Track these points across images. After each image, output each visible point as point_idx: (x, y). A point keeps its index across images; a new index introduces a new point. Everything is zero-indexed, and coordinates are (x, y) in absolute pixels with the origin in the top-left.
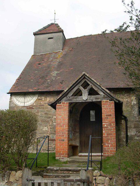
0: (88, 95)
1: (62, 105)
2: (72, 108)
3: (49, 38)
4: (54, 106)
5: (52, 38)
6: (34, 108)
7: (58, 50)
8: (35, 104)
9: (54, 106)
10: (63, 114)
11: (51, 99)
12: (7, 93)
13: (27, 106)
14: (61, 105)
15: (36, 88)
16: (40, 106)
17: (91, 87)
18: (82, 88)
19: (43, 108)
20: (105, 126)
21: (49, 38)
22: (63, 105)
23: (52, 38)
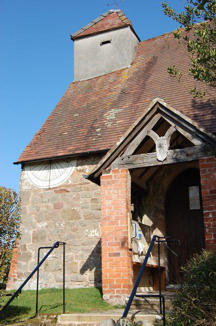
0: (170, 148)
1: (113, 175)
2: (142, 183)
3: (104, 43)
4: (95, 178)
5: (108, 42)
6: (68, 189)
7: (123, 65)
8: (70, 182)
9: (95, 178)
10: (116, 195)
11: (89, 169)
12: (15, 163)
13: (57, 188)
14: (111, 177)
15: (71, 148)
16: (80, 184)
17: (174, 130)
18: (154, 135)
19: (88, 190)
20: (211, 216)
21: (104, 43)
22: (115, 176)
23: (108, 42)
